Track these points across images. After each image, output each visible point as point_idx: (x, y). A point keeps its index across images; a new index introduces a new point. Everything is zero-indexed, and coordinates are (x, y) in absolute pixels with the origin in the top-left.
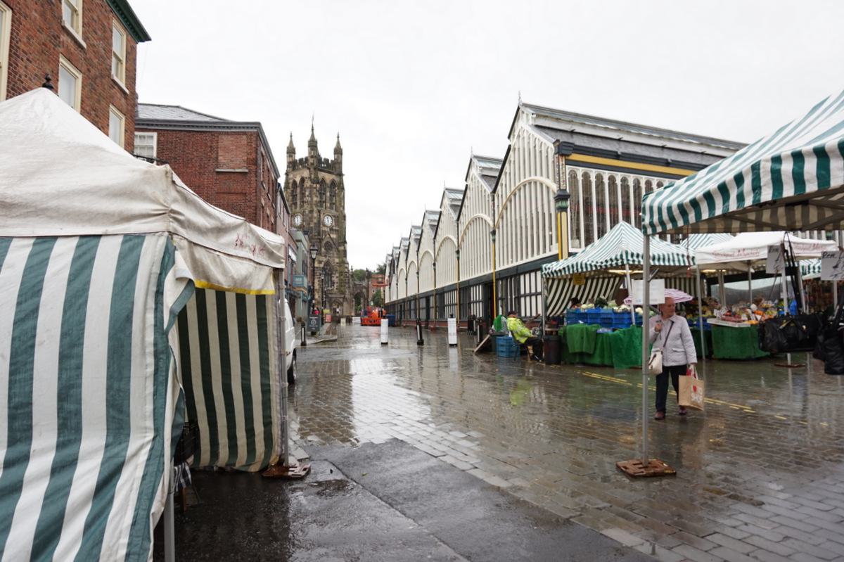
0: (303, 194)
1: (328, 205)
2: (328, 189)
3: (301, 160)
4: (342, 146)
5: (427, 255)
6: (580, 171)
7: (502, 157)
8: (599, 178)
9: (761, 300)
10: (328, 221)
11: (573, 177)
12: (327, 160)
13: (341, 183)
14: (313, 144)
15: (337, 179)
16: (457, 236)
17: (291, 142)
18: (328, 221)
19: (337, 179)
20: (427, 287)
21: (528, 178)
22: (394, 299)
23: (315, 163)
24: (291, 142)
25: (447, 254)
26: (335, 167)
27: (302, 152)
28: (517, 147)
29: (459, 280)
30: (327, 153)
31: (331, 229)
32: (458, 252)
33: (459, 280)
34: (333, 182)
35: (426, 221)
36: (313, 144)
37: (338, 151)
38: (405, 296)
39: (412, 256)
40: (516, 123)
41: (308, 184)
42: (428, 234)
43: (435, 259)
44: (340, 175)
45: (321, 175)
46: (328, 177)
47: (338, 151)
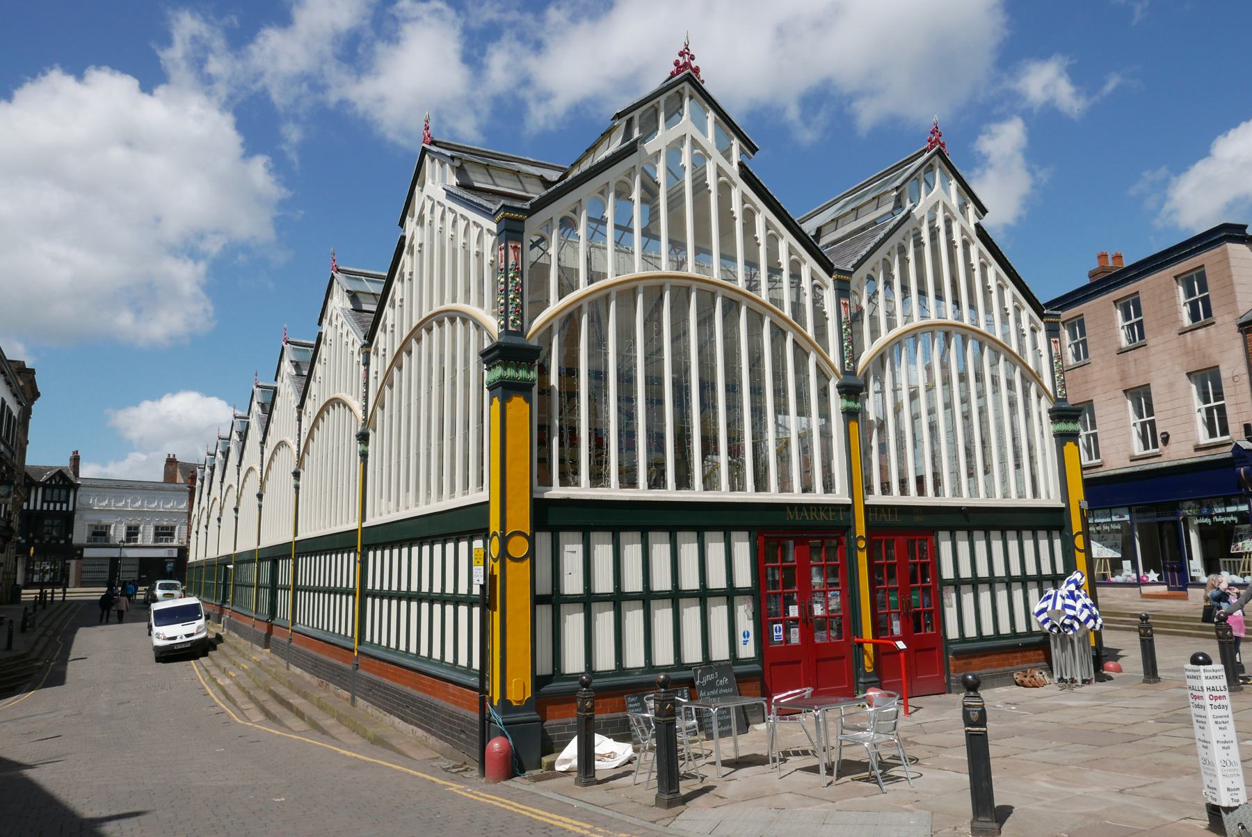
5: (335, 414)
7: (313, 342)
16: (362, 389)
21: (448, 305)
22: (201, 557)
28: (416, 243)
29: (363, 518)
32: (363, 438)
33: (363, 518)
40: (418, 188)
43: (368, 422)
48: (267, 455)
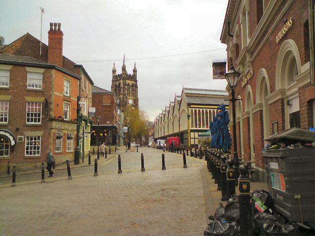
0: (120, 90)
1: (131, 95)
2: (131, 88)
3: (119, 75)
4: (116, 68)
5: (184, 113)
6: (194, 109)
8: (206, 111)
9: (264, 212)
10: (131, 102)
11: (192, 111)
12: (130, 75)
13: (136, 84)
14: (124, 69)
15: (134, 83)
17: (114, 67)
18: (131, 102)
19: (134, 83)
20: (176, 131)
23: (124, 76)
24: (114, 67)
25: (177, 124)
26: (133, 78)
27: (119, 72)
30: (130, 72)
31: (132, 105)
34: (133, 85)
35: (183, 93)
36: (124, 69)
37: (135, 71)
38: (178, 131)
39: (176, 112)
41: (122, 85)
42: (177, 107)
44: (136, 81)
45: (128, 82)
46: (131, 82)
47: (135, 71)
48: (180, 112)
